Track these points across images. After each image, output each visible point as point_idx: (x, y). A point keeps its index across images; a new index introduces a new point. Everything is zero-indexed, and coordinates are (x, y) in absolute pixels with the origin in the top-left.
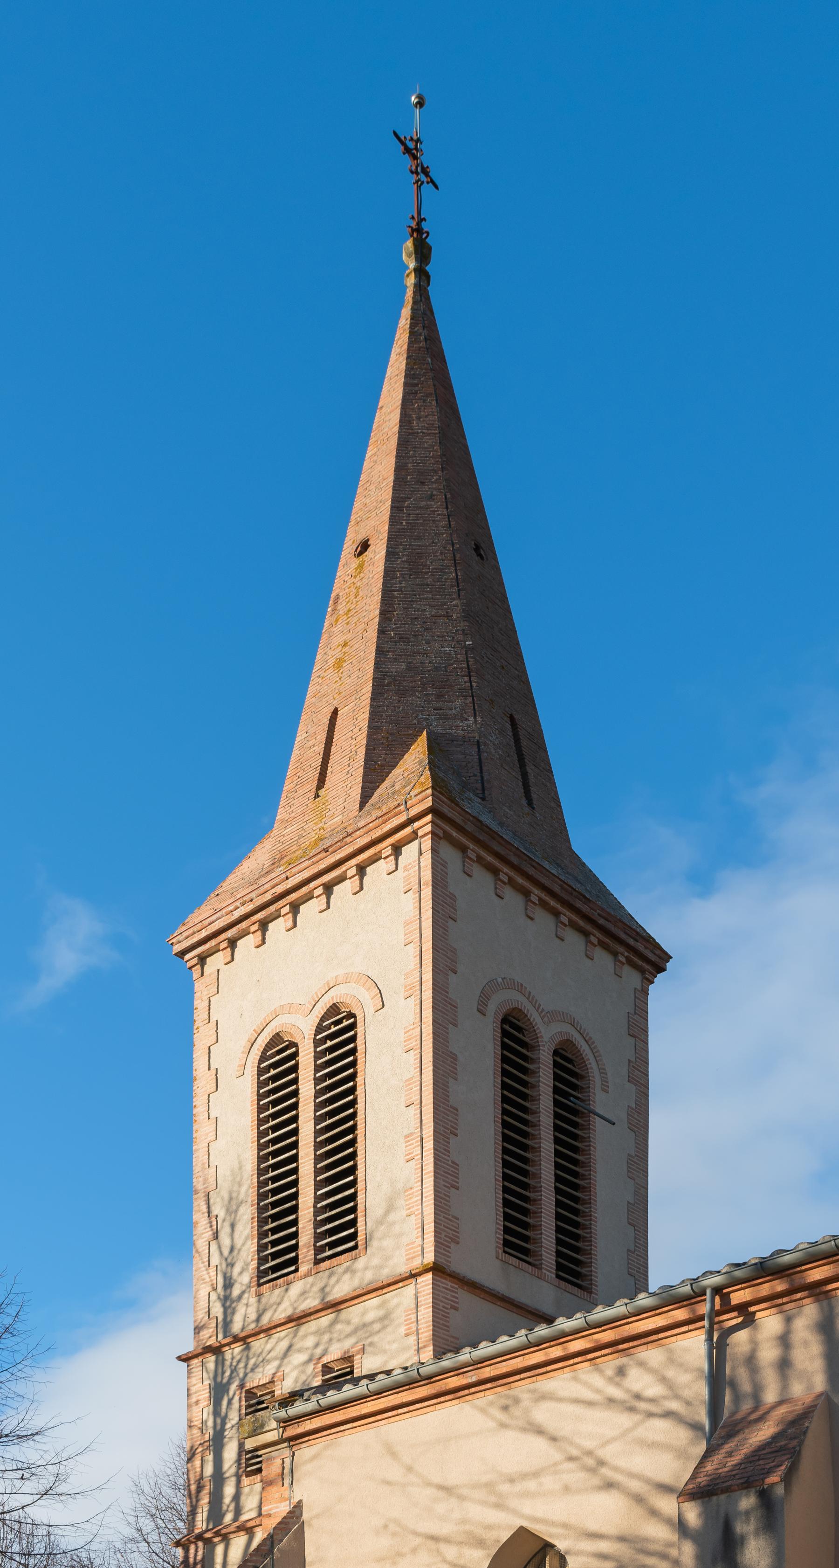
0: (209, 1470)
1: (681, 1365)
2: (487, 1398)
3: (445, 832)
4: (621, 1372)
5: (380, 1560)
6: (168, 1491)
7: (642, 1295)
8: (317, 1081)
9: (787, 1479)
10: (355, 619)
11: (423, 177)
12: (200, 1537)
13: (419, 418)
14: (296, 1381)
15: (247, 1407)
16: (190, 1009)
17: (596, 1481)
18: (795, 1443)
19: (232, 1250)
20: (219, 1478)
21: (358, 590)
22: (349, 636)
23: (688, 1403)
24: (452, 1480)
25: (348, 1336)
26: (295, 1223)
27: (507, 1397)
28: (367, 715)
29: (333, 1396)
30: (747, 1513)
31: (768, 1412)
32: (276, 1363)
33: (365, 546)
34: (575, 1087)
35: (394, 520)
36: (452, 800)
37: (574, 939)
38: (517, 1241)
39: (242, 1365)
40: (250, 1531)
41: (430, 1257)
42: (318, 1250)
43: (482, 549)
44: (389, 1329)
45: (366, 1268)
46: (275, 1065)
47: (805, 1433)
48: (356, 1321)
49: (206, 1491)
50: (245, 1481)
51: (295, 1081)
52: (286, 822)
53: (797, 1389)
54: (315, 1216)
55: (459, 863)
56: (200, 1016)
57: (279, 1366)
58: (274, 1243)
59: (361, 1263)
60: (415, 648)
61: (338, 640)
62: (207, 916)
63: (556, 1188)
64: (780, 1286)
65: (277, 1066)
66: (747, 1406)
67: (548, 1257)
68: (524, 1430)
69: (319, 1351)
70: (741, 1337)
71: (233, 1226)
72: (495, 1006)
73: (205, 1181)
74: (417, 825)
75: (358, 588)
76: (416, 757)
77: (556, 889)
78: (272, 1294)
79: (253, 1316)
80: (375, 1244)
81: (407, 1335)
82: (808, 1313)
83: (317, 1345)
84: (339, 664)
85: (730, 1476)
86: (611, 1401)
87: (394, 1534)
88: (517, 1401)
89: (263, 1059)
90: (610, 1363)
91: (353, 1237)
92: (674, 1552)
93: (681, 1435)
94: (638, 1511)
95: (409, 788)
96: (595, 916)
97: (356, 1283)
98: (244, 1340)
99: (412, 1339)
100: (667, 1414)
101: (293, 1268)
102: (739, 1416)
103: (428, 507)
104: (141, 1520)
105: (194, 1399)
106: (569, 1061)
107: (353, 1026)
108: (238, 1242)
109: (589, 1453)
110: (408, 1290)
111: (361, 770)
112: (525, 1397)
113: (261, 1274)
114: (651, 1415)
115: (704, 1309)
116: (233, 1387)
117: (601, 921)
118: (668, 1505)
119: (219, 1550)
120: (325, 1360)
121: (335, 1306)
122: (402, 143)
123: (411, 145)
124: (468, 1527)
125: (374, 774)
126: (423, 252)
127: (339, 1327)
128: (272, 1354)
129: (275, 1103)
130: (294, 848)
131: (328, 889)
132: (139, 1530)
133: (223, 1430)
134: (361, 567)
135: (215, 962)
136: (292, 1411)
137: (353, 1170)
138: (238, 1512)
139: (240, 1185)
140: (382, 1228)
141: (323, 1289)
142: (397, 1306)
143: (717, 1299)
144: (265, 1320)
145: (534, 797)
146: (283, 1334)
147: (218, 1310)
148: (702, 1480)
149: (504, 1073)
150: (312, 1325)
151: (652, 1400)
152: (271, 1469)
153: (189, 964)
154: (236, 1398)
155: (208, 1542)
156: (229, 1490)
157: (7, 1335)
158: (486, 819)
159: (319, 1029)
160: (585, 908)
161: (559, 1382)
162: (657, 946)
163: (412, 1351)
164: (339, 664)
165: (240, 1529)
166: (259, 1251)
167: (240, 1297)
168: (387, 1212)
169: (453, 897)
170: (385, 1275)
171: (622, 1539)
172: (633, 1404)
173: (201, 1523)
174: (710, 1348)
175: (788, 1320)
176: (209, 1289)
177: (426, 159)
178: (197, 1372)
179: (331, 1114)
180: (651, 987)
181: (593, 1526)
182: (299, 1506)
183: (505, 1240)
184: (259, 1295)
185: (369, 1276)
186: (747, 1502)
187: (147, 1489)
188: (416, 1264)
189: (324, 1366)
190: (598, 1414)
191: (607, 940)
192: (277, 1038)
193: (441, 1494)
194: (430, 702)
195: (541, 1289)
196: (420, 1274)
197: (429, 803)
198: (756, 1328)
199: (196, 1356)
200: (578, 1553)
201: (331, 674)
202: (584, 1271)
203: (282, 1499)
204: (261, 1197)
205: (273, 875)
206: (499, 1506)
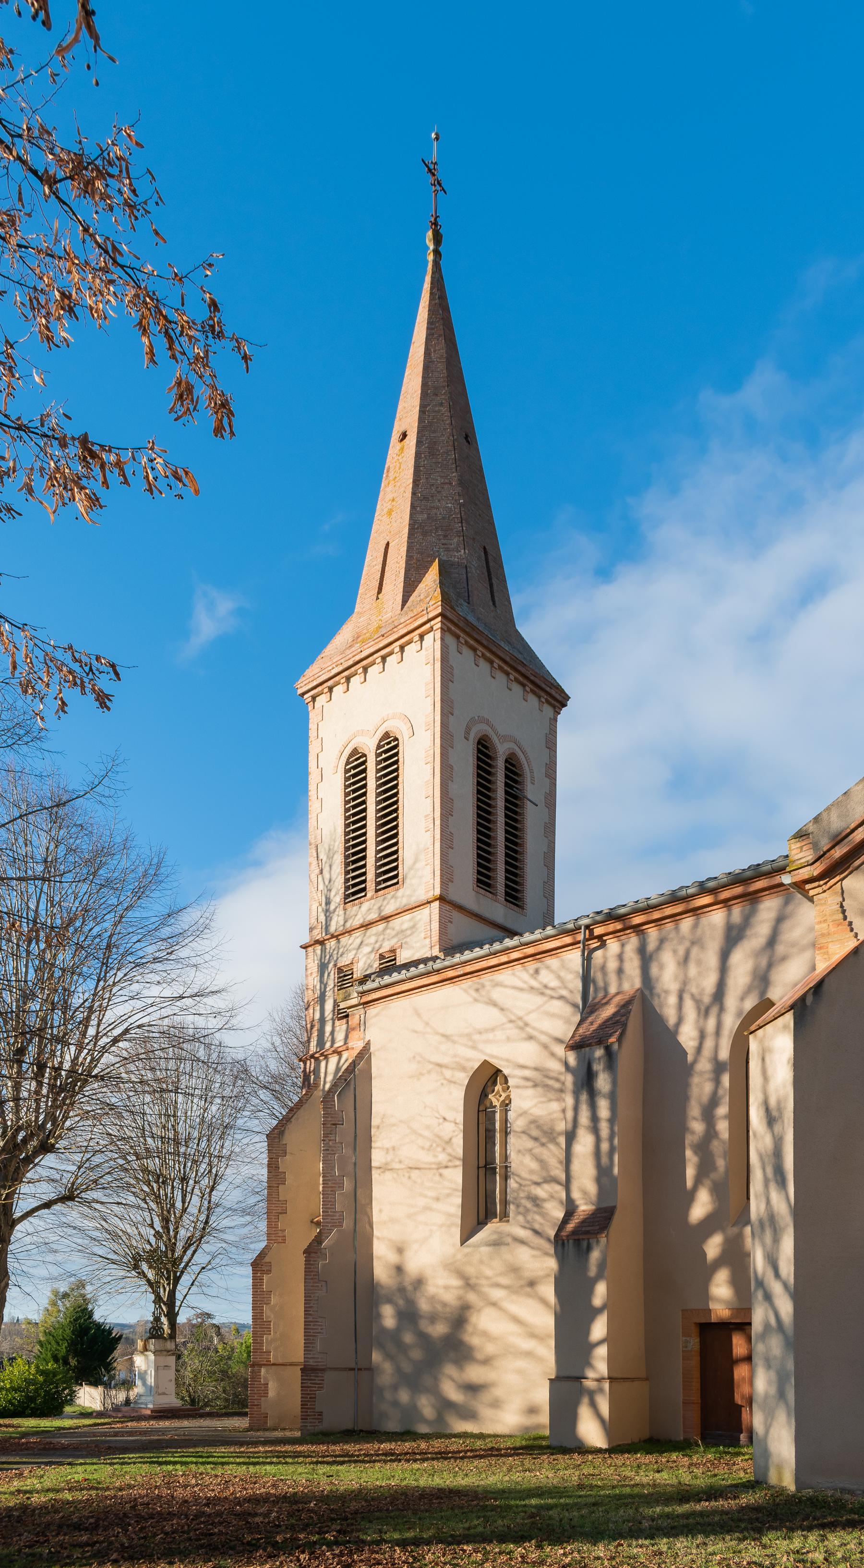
0: (317, 1016)
1: (568, 969)
2: (467, 983)
3: (448, 628)
4: (537, 971)
5: (411, 1077)
6: (288, 1020)
7: (549, 928)
8: (378, 779)
9: (620, 1040)
10: (399, 484)
11: (438, 188)
12: (312, 1056)
13: (435, 351)
14: (365, 963)
15: (339, 978)
16: (307, 729)
17: (524, 1035)
18: (624, 1018)
19: (330, 881)
20: (322, 1020)
21: (400, 463)
22: (395, 495)
23: (571, 992)
24: (449, 1032)
25: (393, 937)
26: (364, 866)
27: (478, 983)
28: (405, 548)
29: (387, 979)
30: (599, 1059)
31: (611, 999)
32: (354, 952)
33: (404, 435)
34: (516, 782)
35: (421, 420)
36: (452, 608)
37: (517, 689)
38: (484, 880)
39: (335, 952)
40: (339, 1054)
41: (437, 892)
42: (378, 884)
43: (469, 438)
44: (416, 934)
45: (403, 896)
46: (354, 768)
47: (630, 1012)
48: (397, 928)
49: (316, 1028)
50: (337, 1023)
51: (365, 778)
52: (361, 614)
53: (626, 986)
54: (376, 862)
55: (455, 646)
56: (312, 734)
57: (356, 954)
58: (354, 878)
59: (400, 893)
60: (432, 505)
61: (389, 497)
62: (316, 672)
63: (506, 845)
64: (618, 926)
65: (355, 767)
66: (601, 994)
67: (501, 888)
68: (487, 1003)
69: (377, 946)
70: (598, 954)
71: (331, 866)
72: (473, 736)
73: (315, 837)
74: (432, 623)
75: (400, 463)
76: (432, 577)
77: (508, 659)
78: (352, 909)
79: (342, 923)
80: (408, 881)
81: (425, 938)
82: (633, 941)
83: (376, 942)
84: (390, 512)
85: (591, 1037)
86: (532, 988)
87: (419, 1062)
88: (483, 986)
89: (347, 763)
90: (532, 966)
91: (396, 876)
92: (562, 1078)
93: (568, 1010)
94: (545, 1053)
95: (428, 599)
96: (528, 675)
97: (397, 905)
98: (336, 937)
99: (428, 940)
100: (561, 998)
101: (363, 894)
102: (596, 1001)
103: (439, 411)
104: (274, 1038)
105: (309, 972)
106: (513, 766)
107: (396, 746)
108: (334, 877)
109: (520, 1018)
110: (425, 912)
111: (402, 584)
112: (487, 984)
113: (346, 896)
114: (552, 997)
115: (580, 937)
116: (331, 965)
117: (532, 678)
118: (560, 1050)
119: (323, 1064)
120: (381, 951)
121: (386, 919)
122: (427, 166)
123: (432, 167)
124: (457, 1059)
125: (410, 586)
126: (438, 239)
127: (388, 931)
128: (352, 946)
129: (354, 791)
130: (365, 631)
131: (384, 659)
132: (273, 1044)
133: (325, 991)
134: (402, 449)
135: (321, 700)
136: (366, 987)
137: (396, 835)
138: (333, 1042)
139: (335, 841)
140: (412, 872)
141: (379, 908)
142: (420, 920)
143: (587, 931)
144: (348, 925)
145: (496, 599)
146: (358, 934)
147: (322, 918)
148: (577, 1038)
149: (479, 775)
150: (374, 930)
151: (553, 989)
152: (354, 1021)
153: (306, 701)
154: (332, 972)
155: (317, 1059)
156: (328, 1028)
157: (206, 931)
158: (471, 619)
159: (379, 747)
160: (523, 670)
161: (505, 976)
162: (563, 691)
163: (428, 948)
164: (390, 512)
165: (334, 1052)
166: (345, 883)
167: (335, 910)
168: (415, 863)
169: (452, 667)
170: (413, 901)
171: (536, 1069)
172: (542, 991)
173: (313, 1047)
174: (583, 960)
175: (623, 945)
176: (318, 904)
177: (439, 175)
178: (311, 954)
179: (385, 800)
180: (559, 716)
181: (522, 1061)
182: (368, 1043)
183: (478, 879)
184: (345, 910)
185: (404, 901)
186: (599, 1053)
187: (277, 1019)
188: (430, 896)
189: (380, 955)
190: (526, 996)
191: (535, 689)
192: (355, 751)
193: (443, 1039)
194: (440, 540)
195: (498, 910)
196: (432, 902)
197: (439, 610)
198: (606, 950)
199: (311, 946)
200: (514, 1077)
201: (385, 518)
202: (519, 895)
203: (360, 1039)
204: (347, 849)
205: (353, 649)
206: (474, 1048)
